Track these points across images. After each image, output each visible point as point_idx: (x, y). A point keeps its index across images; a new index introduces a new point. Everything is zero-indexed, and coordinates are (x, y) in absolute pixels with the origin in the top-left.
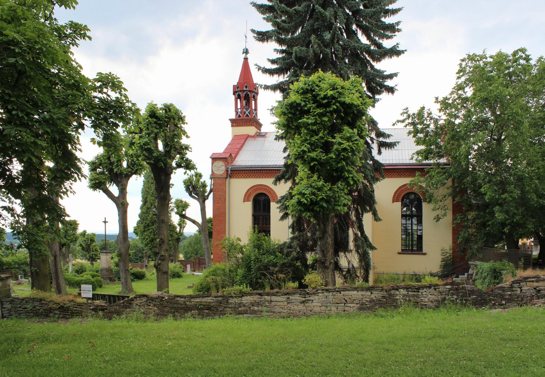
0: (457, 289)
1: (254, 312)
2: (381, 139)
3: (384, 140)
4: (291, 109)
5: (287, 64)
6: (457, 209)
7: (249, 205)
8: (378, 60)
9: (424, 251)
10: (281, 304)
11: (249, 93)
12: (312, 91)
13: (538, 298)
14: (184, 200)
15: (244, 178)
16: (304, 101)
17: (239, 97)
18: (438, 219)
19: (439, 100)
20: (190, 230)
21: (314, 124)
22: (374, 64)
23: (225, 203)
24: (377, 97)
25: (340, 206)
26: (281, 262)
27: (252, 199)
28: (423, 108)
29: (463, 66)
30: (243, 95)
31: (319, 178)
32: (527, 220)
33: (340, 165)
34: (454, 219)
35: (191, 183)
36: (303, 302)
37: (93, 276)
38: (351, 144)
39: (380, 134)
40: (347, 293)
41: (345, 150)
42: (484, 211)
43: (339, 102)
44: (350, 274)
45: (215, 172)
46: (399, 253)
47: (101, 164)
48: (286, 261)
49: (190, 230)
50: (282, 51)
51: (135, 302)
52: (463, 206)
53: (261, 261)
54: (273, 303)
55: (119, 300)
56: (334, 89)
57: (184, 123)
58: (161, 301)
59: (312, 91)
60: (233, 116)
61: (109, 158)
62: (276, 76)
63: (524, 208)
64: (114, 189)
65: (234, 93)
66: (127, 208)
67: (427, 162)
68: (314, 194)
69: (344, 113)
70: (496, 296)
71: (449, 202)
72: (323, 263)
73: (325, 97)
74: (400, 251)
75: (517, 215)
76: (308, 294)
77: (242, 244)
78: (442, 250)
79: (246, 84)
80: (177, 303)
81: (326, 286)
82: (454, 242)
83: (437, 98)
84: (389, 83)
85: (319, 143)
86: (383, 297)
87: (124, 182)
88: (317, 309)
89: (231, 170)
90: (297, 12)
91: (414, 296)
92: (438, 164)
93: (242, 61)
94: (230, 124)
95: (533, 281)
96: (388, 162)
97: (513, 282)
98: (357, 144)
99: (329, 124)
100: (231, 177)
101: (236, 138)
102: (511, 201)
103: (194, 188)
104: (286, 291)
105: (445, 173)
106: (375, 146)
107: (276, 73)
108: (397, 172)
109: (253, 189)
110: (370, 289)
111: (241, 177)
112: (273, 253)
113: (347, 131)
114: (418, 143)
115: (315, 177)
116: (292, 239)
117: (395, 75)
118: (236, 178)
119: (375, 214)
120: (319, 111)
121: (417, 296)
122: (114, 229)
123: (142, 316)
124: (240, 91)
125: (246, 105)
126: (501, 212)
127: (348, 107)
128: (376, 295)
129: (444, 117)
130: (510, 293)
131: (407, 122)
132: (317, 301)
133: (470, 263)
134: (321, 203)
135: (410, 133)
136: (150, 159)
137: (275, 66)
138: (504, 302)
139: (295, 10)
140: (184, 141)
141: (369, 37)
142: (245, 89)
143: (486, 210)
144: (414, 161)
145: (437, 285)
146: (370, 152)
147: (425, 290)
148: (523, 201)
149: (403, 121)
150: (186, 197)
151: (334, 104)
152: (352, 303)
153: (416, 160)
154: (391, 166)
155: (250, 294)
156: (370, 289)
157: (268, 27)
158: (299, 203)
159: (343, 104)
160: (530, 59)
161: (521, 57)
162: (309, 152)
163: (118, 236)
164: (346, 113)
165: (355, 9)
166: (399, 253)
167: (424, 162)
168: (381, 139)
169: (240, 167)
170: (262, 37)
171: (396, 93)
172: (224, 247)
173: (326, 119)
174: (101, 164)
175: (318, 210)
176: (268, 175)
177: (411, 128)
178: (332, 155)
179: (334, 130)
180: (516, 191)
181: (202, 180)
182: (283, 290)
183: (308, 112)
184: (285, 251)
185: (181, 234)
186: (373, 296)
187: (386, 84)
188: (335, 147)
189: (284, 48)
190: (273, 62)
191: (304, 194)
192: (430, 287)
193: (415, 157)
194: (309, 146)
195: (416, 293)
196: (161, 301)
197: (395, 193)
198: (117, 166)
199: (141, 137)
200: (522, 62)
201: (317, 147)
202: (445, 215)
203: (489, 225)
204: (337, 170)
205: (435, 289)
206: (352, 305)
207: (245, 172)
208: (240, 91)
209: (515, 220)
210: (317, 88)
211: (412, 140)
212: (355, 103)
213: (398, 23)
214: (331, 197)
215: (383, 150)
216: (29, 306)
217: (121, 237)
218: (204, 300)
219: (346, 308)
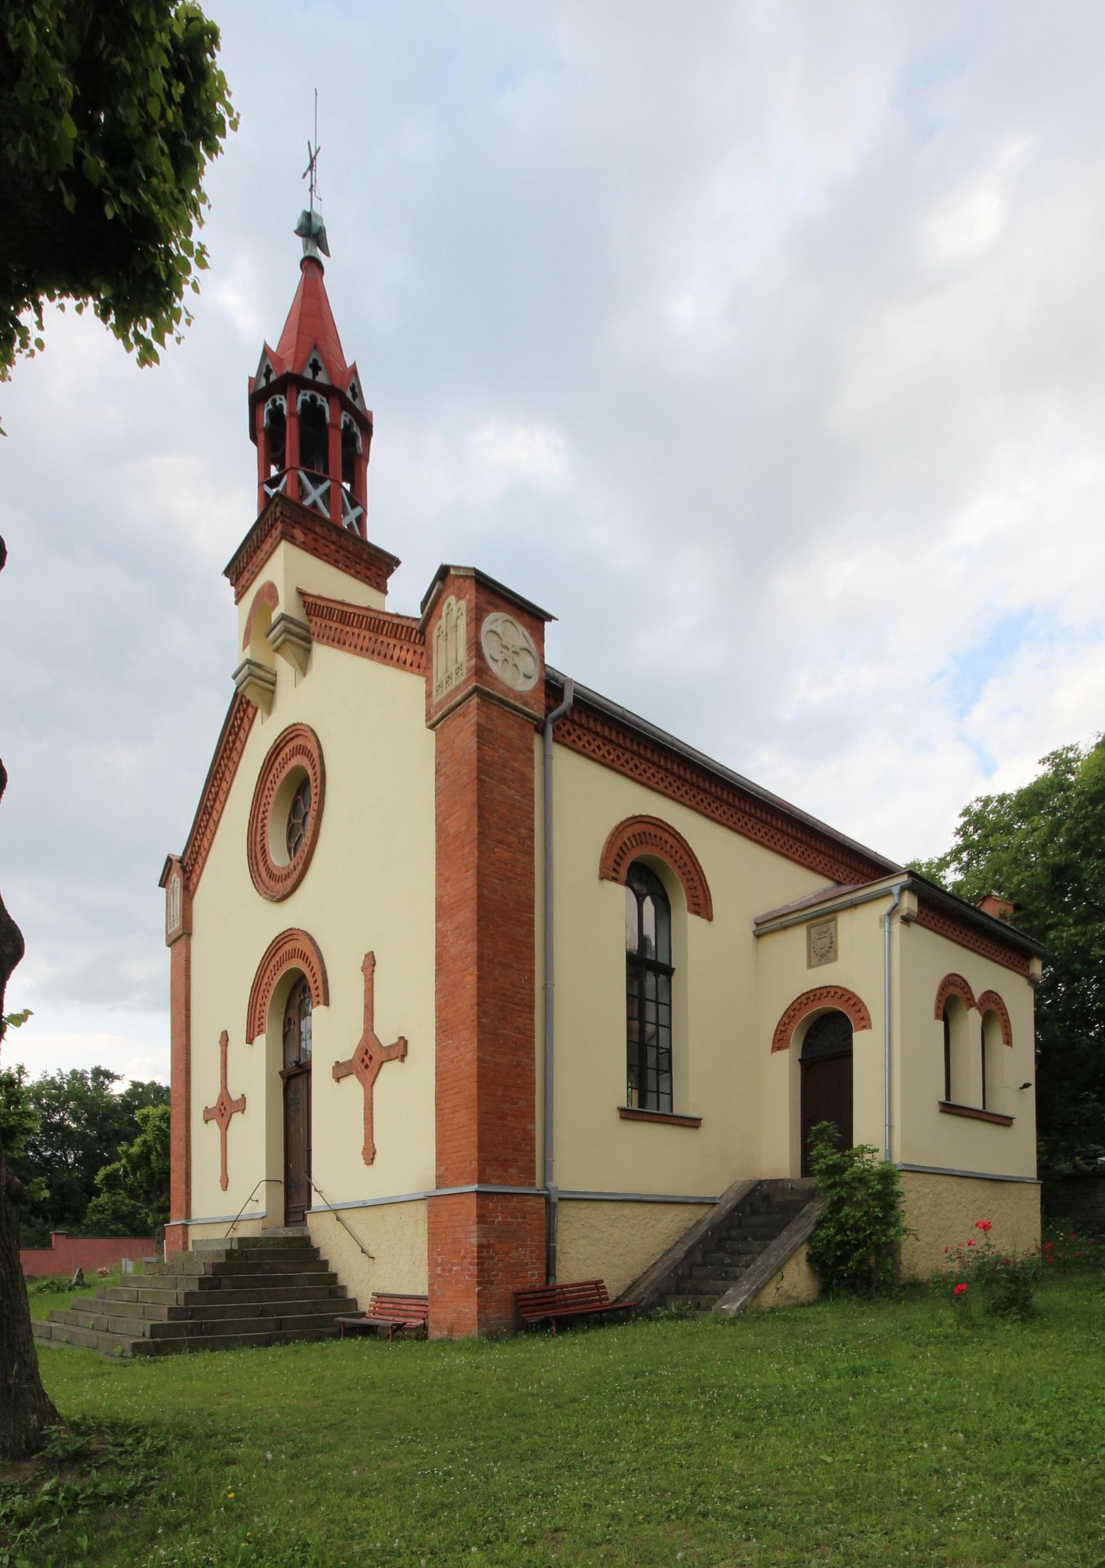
11: (322, 401)
23: (530, 853)
79: (315, 355)
89: (575, 698)
93: (295, 275)
142: (308, 374)
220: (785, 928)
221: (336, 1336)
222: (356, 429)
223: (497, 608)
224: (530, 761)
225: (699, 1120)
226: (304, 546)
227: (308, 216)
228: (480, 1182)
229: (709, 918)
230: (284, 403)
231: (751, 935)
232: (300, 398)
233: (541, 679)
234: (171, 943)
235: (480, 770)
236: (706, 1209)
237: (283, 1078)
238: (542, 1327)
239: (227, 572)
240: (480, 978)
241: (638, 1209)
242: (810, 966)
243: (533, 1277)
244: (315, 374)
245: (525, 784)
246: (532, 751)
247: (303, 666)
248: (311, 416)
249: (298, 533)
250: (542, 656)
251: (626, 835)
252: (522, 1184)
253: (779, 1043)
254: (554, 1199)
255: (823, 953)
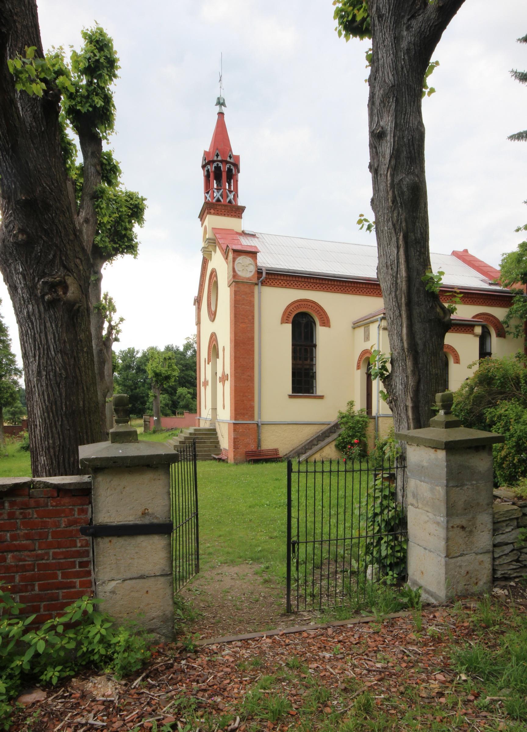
7: (288, 328)
9: (319, 392)
11: (220, 165)
15: (282, 287)
23: (253, 323)
27: (291, 319)
45: (239, 273)
79: (217, 152)
89: (267, 273)
93: (215, 118)
108: (286, 280)
109: (297, 304)
111: (278, 286)
118: (270, 285)
124: (221, 161)
142: (215, 158)
154: (335, 277)
169: (317, 274)
176: (316, 286)
207: (336, 283)
208: (221, 161)
220: (359, 327)
221: (211, 460)
222: (232, 167)
223: (240, 255)
224: (253, 296)
225: (323, 396)
226: (214, 214)
227: (219, 99)
228: (235, 420)
229: (329, 327)
230: (221, 165)
231: (351, 328)
232: (214, 166)
233: (256, 271)
234: (197, 325)
235: (235, 303)
236: (326, 426)
237: (431, 269)
238: (256, 461)
239: (199, 217)
240: (235, 363)
241: (295, 426)
242: (365, 341)
243: (253, 447)
244: (217, 157)
245: (251, 304)
246: (253, 292)
247: (215, 251)
248: (218, 168)
249: (212, 211)
250: (256, 264)
251: (291, 308)
252: (250, 420)
253: (358, 367)
254: (260, 424)
255: (367, 338)
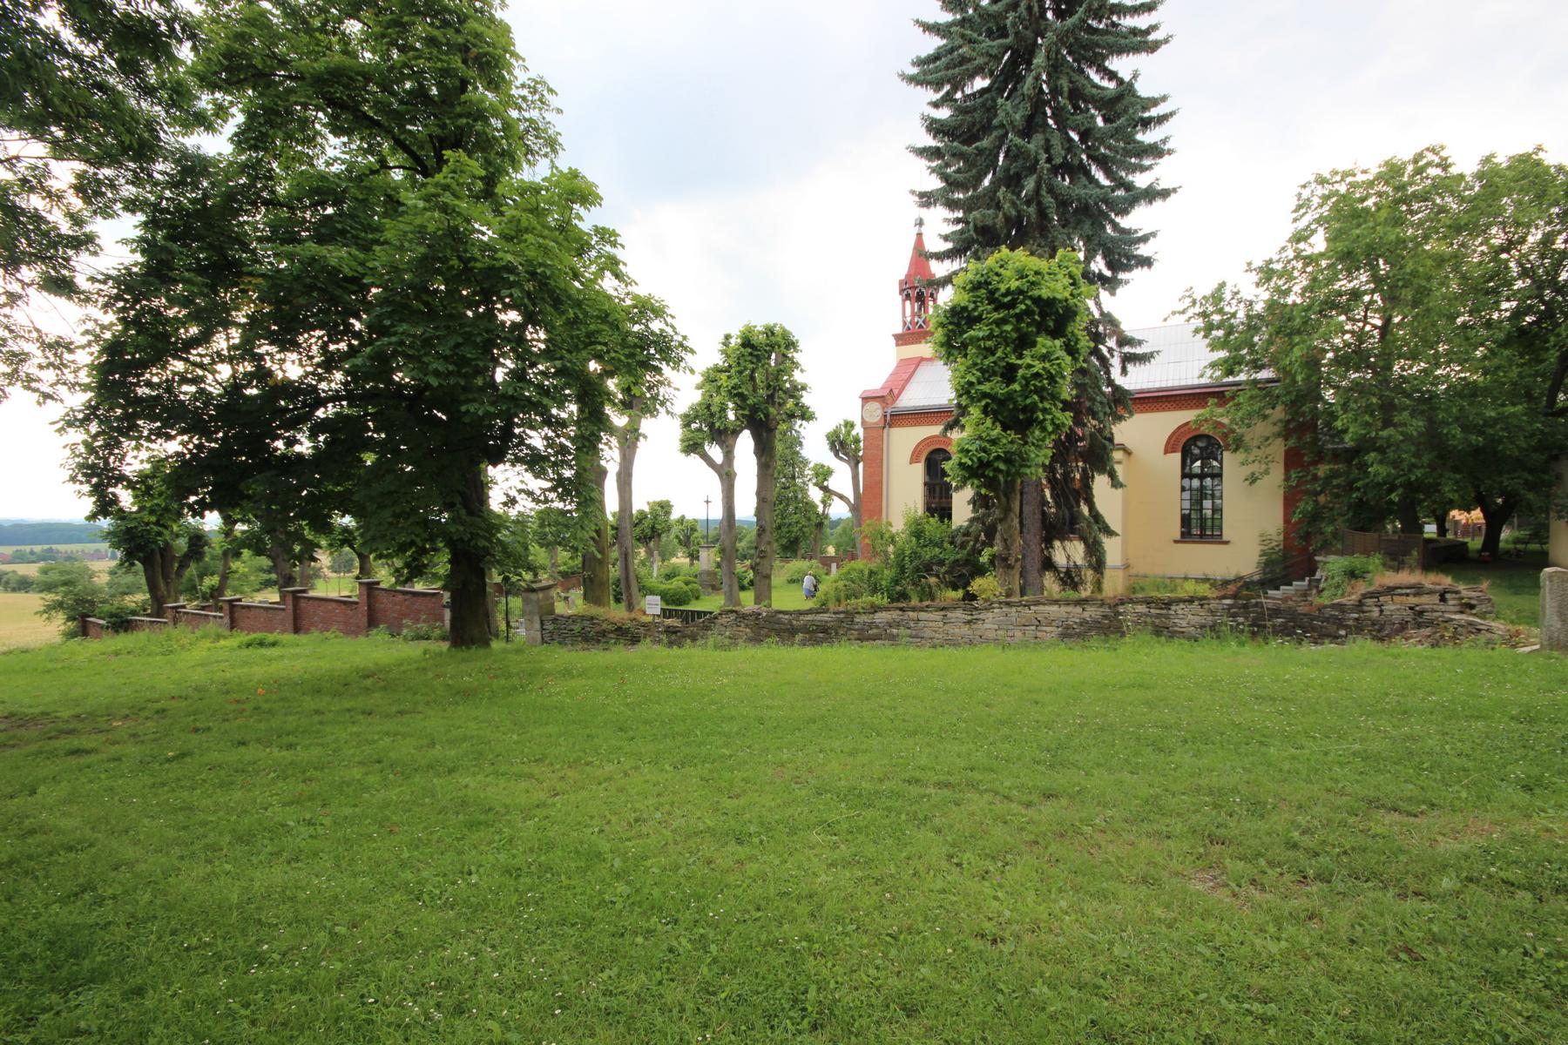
0: (1245, 606)
1: (893, 638)
2: (1127, 349)
3: (1132, 350)
4: (953, 316)
5: (964, 241)
6: (1292, 460)
8: (1124, 212)
9: (1225, 538)
10: (934, 624)
12: (988, 283)
13: (1419, 626)
14: (826, 464)
16: (975, 302)
17: (908, 297)
18: (1253, 479)
19: (1253, 267)
20: (839, 511)
21: (990, 337)
22: (1118, 219)
24: (1122, 276)
25: (1029, 467)
26: (952, 558)
28: (1222, 285)
29: (1305, 196)
30: (913, 293)
31: (993, 423)
32: (1441, 476)
33: (1028, 401)
34: (1287, 479)
35: (838, 437)
36: (969, 622)
37: (687, 583)
38: (1047, 365)
39: (1124, 341)
40: (1041, 608)
41: (1037, 375)
42: (1349, 462)
43: (1031, 298)
44: (1070, 579)
46: (1176, 542)
47: (696, 417)
48: (959, 556)
49: (839, 511)
50: (958, 221)
51: (719, 621)
52: (1304, 455)
53: (920, 557)
54: (921, 624)
55: (699, 618)
56: (1022, 278)
57: (797, 351)
58: (757, 619)
59: (988, 283)
60: (899, 330)
61: (708, 407)
62: (947, 263)
63: (1435, 453)
64: (716, 452)
65: (902, 291)
66: (733, 480)
67: (1231, 379)
68: (984, 450)
69: (1040, 314)
70: (1327, 620)
71: (1278, 449)
72: (1005, 560)
73: (1008, 292)
74: (1178, 537)
75: (1418, 468)
76: (976, 609)
77: (894, 530)
78: (1261, 536)
80: (779, 622)
81: (1008, 596)
82: (1287, 521)
83: (1249, 264)
84: (1143, 250)
85: (996, 369)
86: (1105, 617)
87: (730, 442)
88: (991, 635)
90: (980, 151)
91: (1158, 616)
92: (1255, 382)
93: (913, 239)
94: (893, 341)
95: (1407, 595)
96: (1138, 387)
97: (1365, 596)
98: (1059, 364)
99: (1015, 335)
100: (890, 426)
101: (903, 363)
102: (1402, 441)
103: (842, 444)
104: (942, 604)
105: (1265, 397)
106: (1115, 362)
107: (949, 257)
110: (1080, 602)
112: (939, 544)
113: (1044, 343)
114: (1214, 347)
115: (989, 422)
116: (972, 520)
117: (1153, 234)
119: (1112, 475)
120: (996, 316)
121: (1167, 617)
122: (717, 513)
123: (727, 641)
125: (920, 309)
126: (1381, 462)
127: (1046, 305)
128: (1092, 613)
129: (1266, 296)
130: (1356, 615)
131: (1190, 312)
132: (990, 621)
133: (1317, 558)
134: (996, 464)
135: (1197, 331)
136: (743, 409)
137: (949, 245)
138: (1342, 632)
139: (977, 148)
140: (798, 376)
141: (1109, 174)
143: (1353, 459)
144: (1204, 381)
145: (1205, 598)
146: (1108, 373)
147: (1182, 606)
148: (1433, 440)
149: (1183, 312)
150: (827, 458)
151: (1021, 303)
152: (1049, 625)
153: (1211, 377)
155: (887, 609)
156: (1080, 602)
157: (935, 183)
158: (961, 465)
159: (1038, 301)
160: (1450, 165)
161: (1429, 164)
162: (980, 383)
163: (721, 522)
164: (1043, 315)
165: (1083, 129)
166: (1176, 542)
167: (1225, 380)
168: (1127, 349)
170: (927, 199)
171: (1156, 265)
172: (866, 537)
173: (1008, 328)
174: (696, 417)
175: (991, 474)
177: (1199, 322)
178: (1016, 387)
179: (1023, 342)
180: (1414, 422)
181: (854, 433)
182: (937, 603)
183: (979, 319)
184: (959, 540)
185: (825, 516)
186: (1086, 615)
187: (1139, 252)
188: (1021, 372)
189: (960, 214)
190: (946, 238)
191: (968, 451)
192: (1191, 601)
193: (1209, 372)
194: (978, 374)
195: (1164, 612)
196: (757, 619)
197: (1170, 438)
198: (720, 418)
199: (729, 377)
200: (1433, 172)
201: (994, 374)
202: (1267, 472)
203: (1358, 489)
204: (1024, 410)
205: (1202, 605)
206: (1048, 629)
209: (1413, 478)
210: (996, 278)
211: (1201, 343)
212: (1059, 296)
213: (1164, 141)
214: (1013, 453)
215: (1130, 367)
216: (577, 628)
217: (725, 523)
218: (819, 617)
219: (1039, 634)
